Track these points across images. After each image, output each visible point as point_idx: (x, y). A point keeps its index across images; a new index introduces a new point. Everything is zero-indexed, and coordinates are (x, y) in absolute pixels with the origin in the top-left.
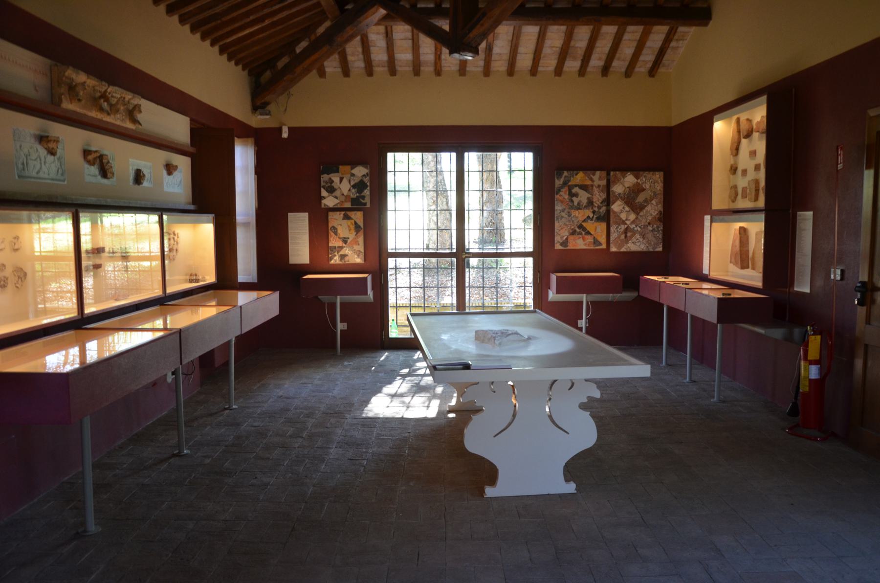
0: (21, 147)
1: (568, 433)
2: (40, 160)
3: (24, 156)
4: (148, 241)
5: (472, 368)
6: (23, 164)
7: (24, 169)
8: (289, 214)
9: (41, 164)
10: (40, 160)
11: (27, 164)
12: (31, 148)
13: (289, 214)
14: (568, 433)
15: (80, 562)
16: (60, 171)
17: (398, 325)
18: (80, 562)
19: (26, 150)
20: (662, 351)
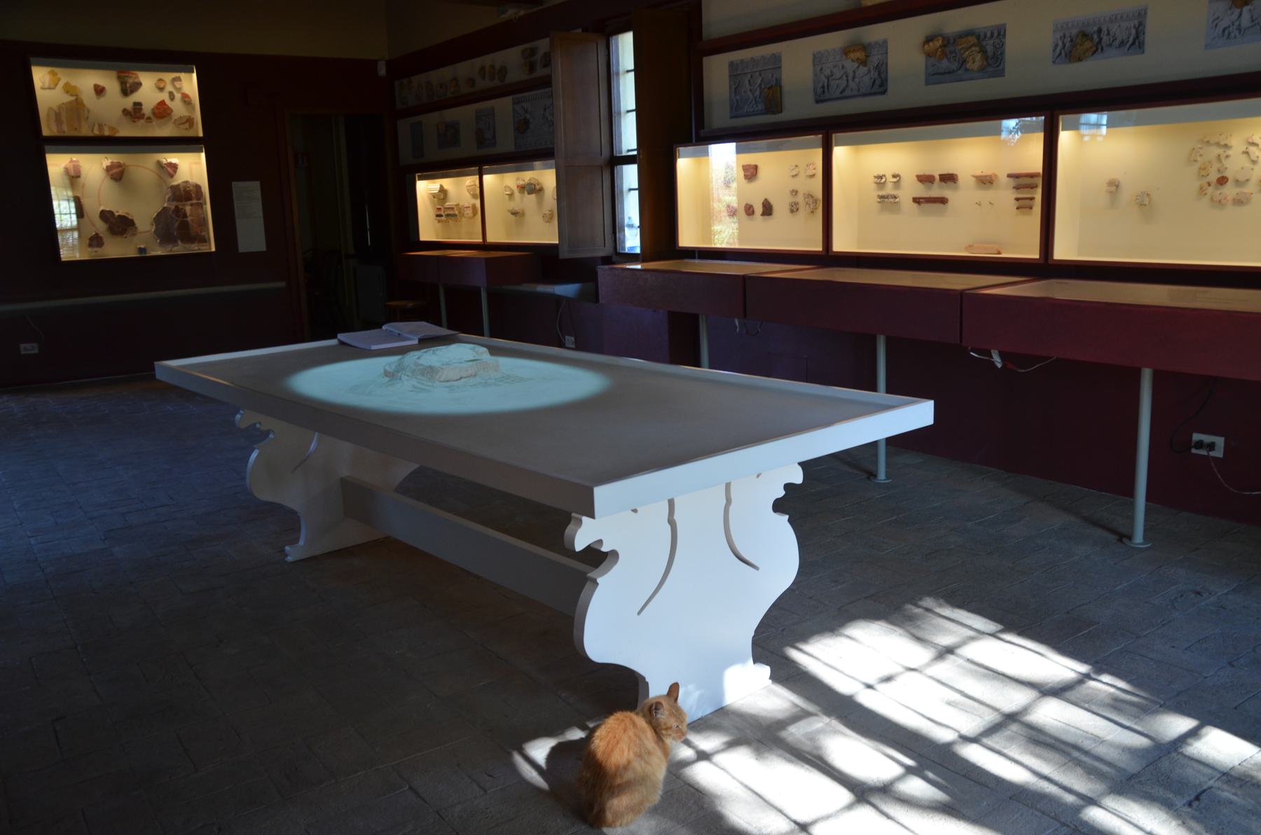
0: (821, 69)
1: (639, 613)
2: (847, 76)
3: (824, 78)
4: (595, 44)
5: (81, 220)
6: (823, 87)
7: (824, 92)
8: (264, 249)
9: (848, 81)
10: (847, 76)
11: (828, 86)
12: (835, 67)
13: (264, 249)
14: (639, 613)
15: (1222, 480)
16: (878, 82)
17: (52, 86)
18: (1222, 480)
19: (827, 72)
20: (1132, 506)
